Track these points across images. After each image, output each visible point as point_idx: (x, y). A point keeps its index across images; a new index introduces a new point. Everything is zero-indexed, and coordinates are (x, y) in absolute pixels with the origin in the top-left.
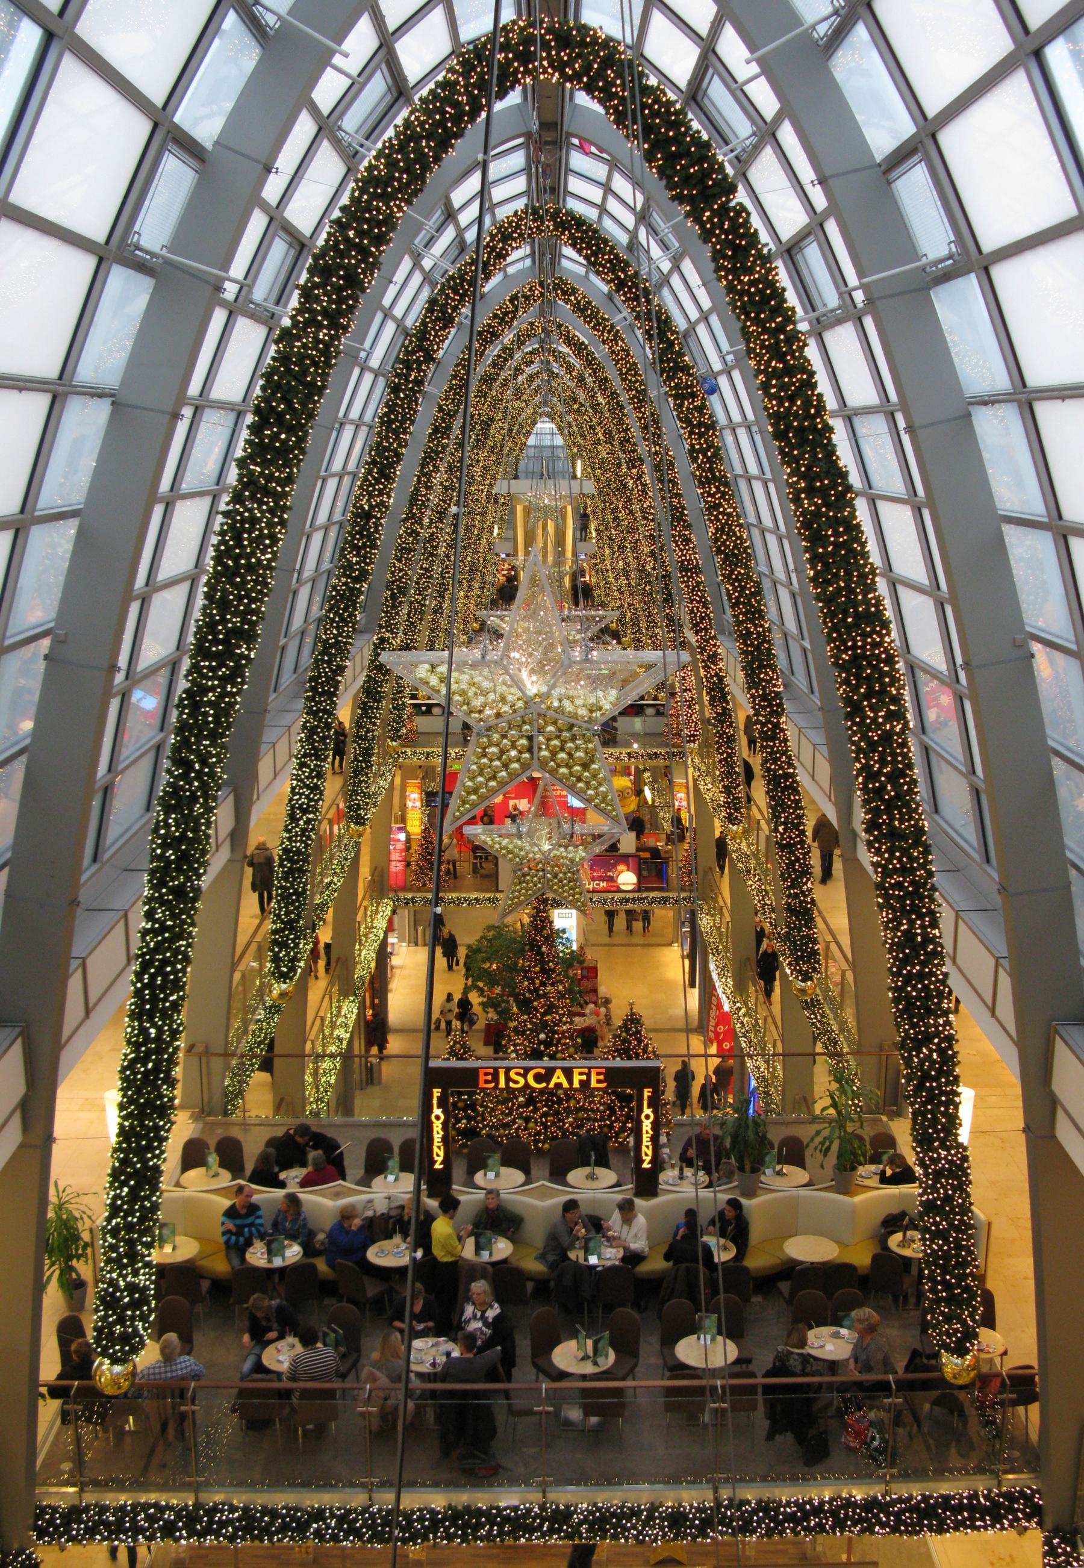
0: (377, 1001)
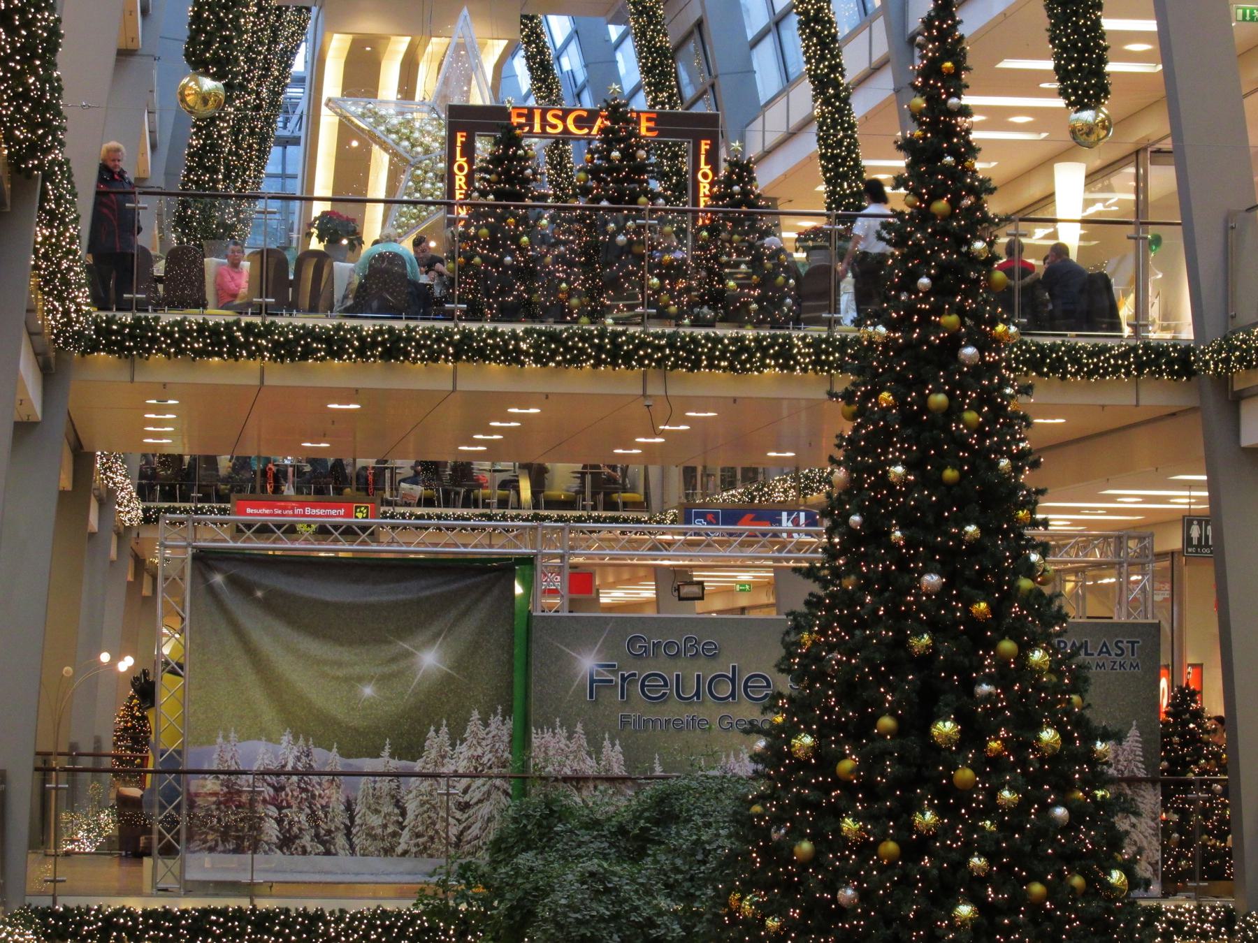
0: (259, 594)
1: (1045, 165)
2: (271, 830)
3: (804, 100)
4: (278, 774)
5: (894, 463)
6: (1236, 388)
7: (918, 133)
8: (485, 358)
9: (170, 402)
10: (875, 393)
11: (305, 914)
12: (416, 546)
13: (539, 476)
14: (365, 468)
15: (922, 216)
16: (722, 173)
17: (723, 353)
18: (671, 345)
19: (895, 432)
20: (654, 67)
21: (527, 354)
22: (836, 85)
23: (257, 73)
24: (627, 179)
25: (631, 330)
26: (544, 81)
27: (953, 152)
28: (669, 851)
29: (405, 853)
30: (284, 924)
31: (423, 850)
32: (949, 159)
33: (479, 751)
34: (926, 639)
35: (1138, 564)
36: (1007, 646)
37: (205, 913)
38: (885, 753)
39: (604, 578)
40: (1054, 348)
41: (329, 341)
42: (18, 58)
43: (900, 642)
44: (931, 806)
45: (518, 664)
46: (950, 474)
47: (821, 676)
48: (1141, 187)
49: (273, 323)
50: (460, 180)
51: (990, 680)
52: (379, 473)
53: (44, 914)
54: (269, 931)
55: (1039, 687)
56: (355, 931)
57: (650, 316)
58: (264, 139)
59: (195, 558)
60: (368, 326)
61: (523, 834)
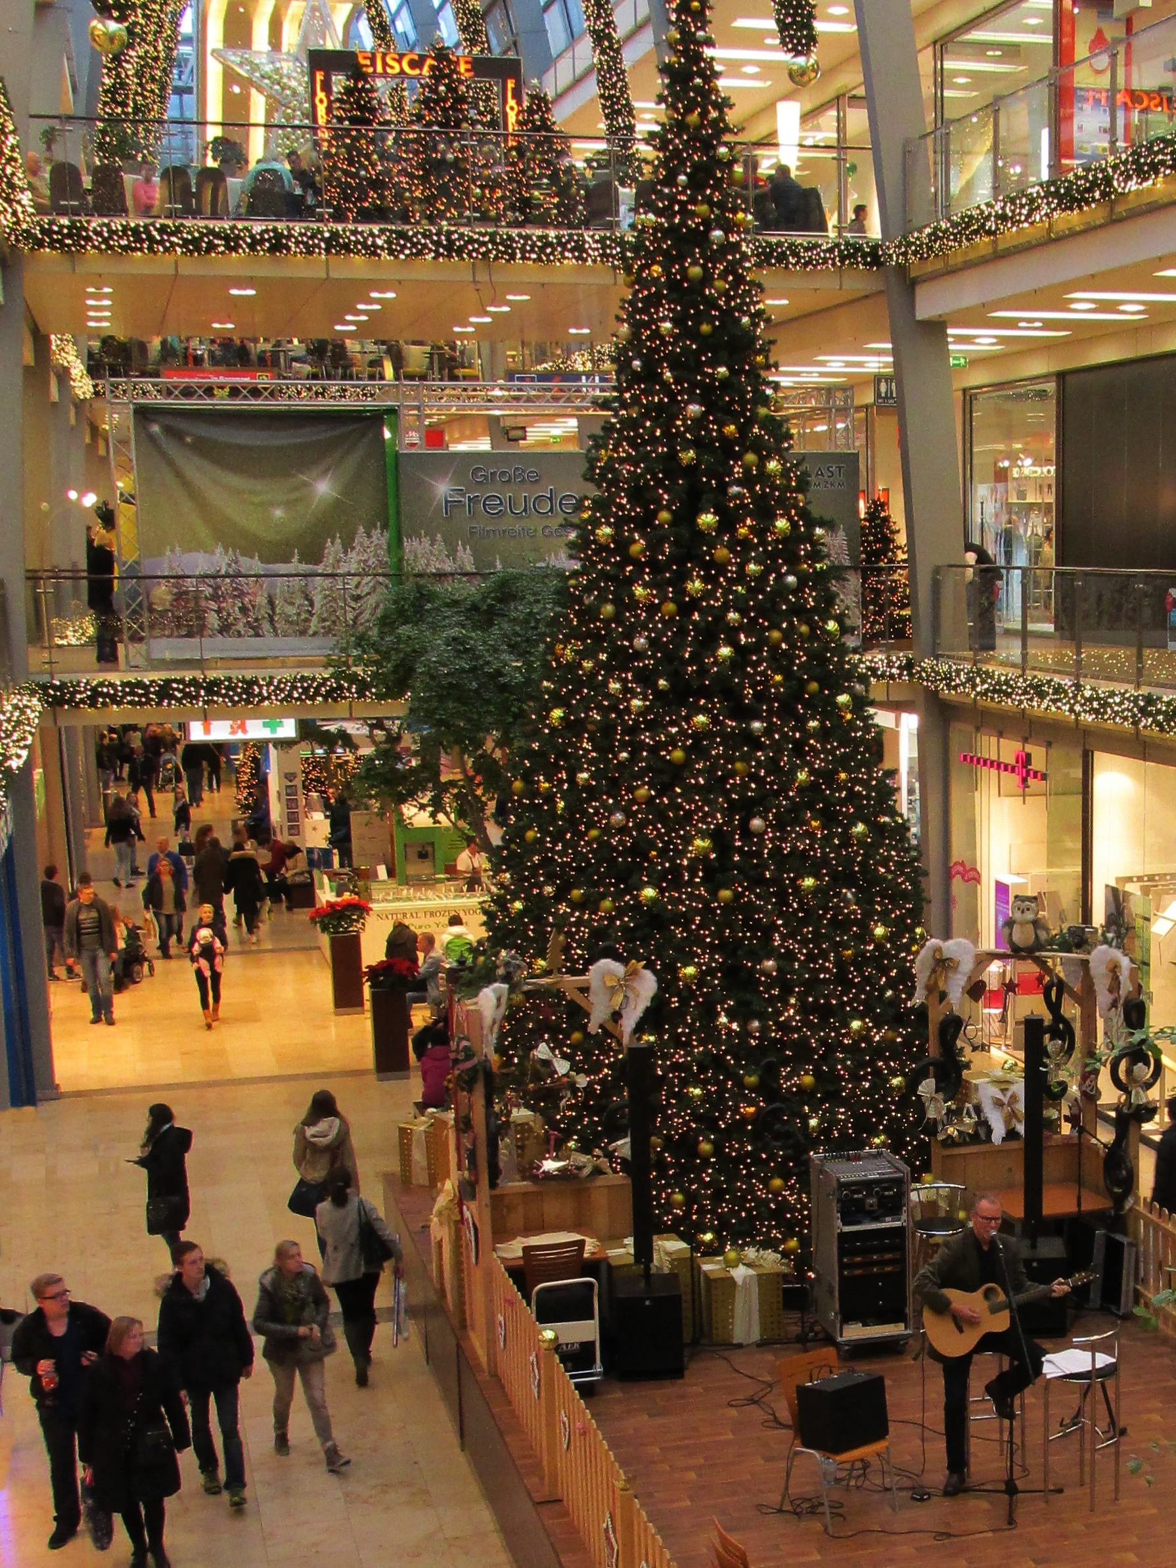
1: (769, 108)
2: (213, 620)
3: (586, 53)
4: (214, 577)
5: (664, 319)
6: (913, 275)
7: (674, 59)
8: (349, 251)
10: (647, 266)
11: (244, 681)
12: (305, 403)
13: (398, 361)
14: (264, 352)
15: (680, 126)
16: (526, 104)
17: (533, 245)
18: (492, 241)
19: (665, 297)
20: (469, 25)
21: (382, 248)
22: (609, 37)
23: (153, 27)
24: (452, 108)
25: (462, 230)
26: (382, 39)
27: (701, 73)
28: (510, 621)
29: (315, 634)
30: (228, 688)
31: (328, 631)
32: (698, 81)
33: (365, 557)
34: (691, 453)
35: (843, 412)
36: (751, 457)
37: (168, 682)
38: (663, 539)
39: (451, 437)
40: (779, 244)
41: (227, 238)
43: (672, 456)
44: (698, 576)
45: (391, 491)
46: (705, 328)
47: (614, 483)
48: (841, 128)
49: (182, 225)
50: (321, 110)
51: (738, 482)
52: (275, 355)
53: (44, 688)
54: (218, 694)
55: (774, 488)
56: (282, 690)
57: (476, 219)
58: (163, 88)
59: (136, 412)
60: (257, 228)
61: (401, 612)
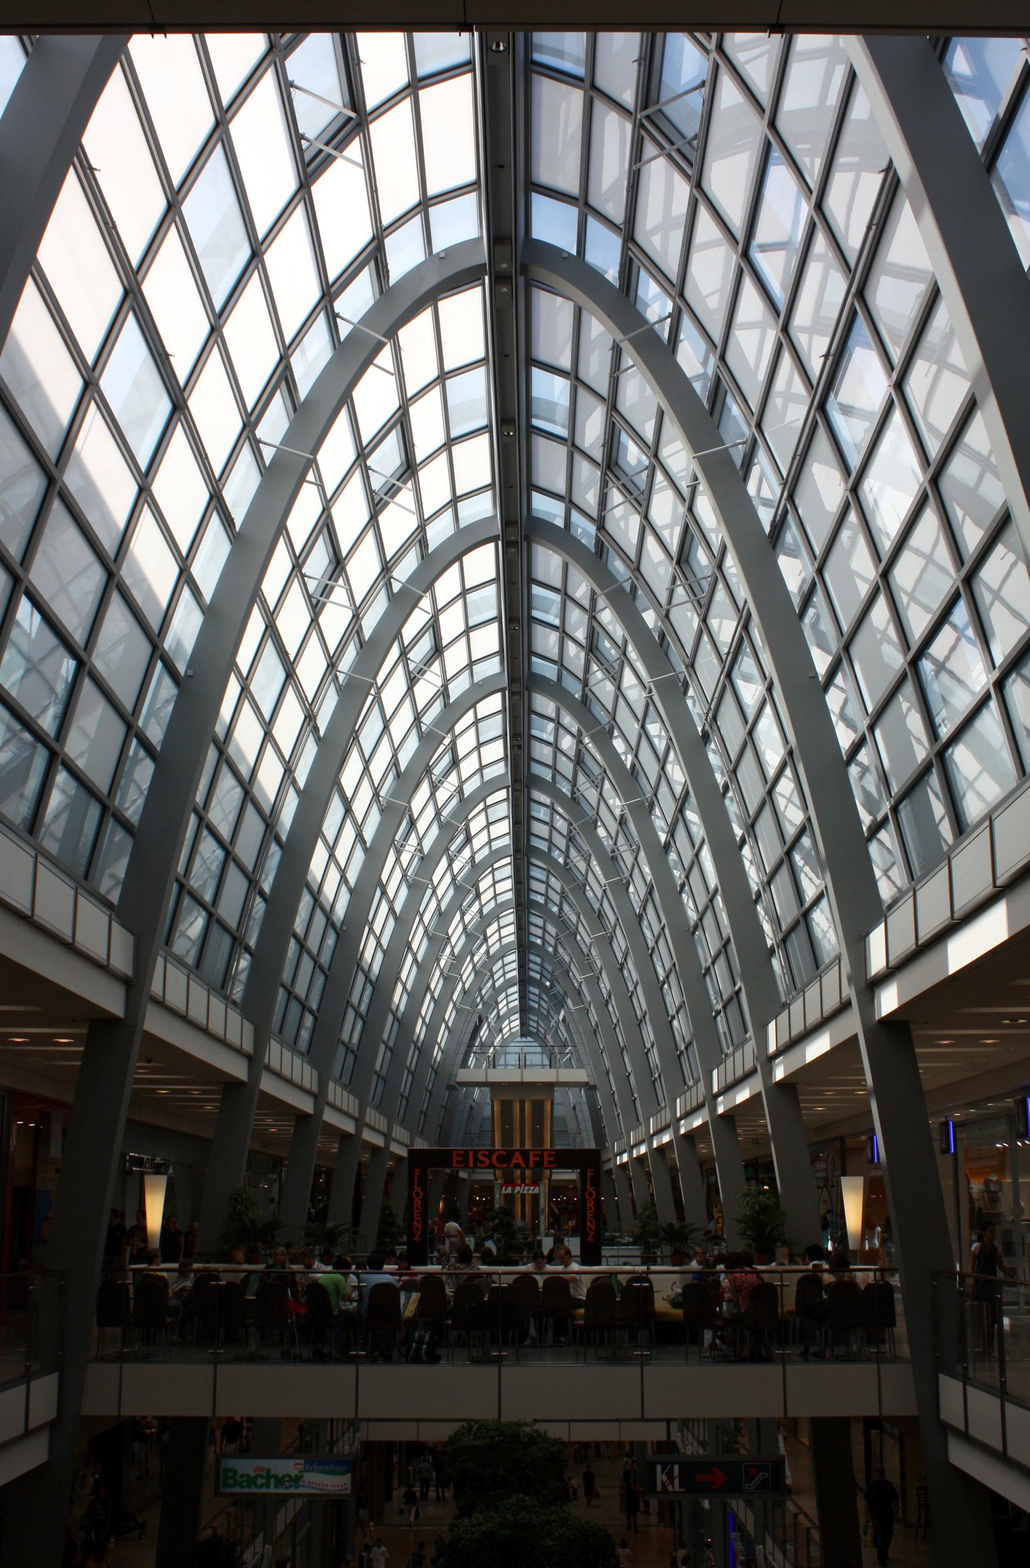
9: (1020, 1021)
42: (718, 1309)
